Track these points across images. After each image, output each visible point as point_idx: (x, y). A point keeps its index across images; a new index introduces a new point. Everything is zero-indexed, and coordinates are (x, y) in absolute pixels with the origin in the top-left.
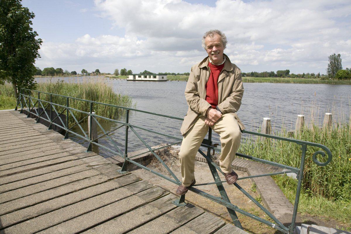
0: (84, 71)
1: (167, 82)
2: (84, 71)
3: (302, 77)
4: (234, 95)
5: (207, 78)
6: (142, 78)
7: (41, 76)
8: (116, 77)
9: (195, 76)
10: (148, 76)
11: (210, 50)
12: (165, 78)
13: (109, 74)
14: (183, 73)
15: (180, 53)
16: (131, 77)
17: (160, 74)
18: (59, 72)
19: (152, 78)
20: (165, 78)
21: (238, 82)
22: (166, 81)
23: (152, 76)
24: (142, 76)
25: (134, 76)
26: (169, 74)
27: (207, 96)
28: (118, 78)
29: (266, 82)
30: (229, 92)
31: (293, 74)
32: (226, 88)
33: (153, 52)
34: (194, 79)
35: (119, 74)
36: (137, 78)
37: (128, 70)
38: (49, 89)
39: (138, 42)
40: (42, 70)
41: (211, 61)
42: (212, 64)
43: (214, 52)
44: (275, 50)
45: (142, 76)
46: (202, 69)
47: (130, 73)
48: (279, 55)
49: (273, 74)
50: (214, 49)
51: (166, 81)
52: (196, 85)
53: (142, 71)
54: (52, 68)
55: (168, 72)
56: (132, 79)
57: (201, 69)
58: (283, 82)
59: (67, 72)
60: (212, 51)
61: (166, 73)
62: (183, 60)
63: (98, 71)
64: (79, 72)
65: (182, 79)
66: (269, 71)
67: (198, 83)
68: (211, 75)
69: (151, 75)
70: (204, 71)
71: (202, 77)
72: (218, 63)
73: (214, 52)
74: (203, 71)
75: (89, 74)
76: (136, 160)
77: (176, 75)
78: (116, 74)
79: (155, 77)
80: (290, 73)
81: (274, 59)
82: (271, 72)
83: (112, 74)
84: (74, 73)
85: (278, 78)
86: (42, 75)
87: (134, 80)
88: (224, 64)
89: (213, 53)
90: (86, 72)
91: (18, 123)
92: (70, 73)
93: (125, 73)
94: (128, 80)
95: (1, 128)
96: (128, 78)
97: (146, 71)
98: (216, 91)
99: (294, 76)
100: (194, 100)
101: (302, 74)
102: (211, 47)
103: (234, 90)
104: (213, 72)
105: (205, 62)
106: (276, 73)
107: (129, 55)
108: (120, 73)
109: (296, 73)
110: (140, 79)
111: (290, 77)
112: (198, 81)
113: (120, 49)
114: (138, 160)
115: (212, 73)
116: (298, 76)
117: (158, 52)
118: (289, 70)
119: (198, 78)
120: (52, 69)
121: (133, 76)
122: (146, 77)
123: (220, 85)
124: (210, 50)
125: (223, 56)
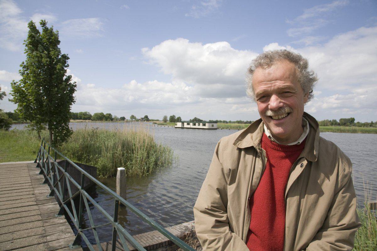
0: (133, 117)
1: (218, 130)
2: (133, 117)
3: (371, 126)
4: (332, 239)
5: (255, 180)
6: (191, 125)
7: (90, 121)
8: (165, 123)
9: (222, 170)
10: (197, 124)
11: (263, 105)
12: (215, 125)
13: (157, 120)
14: (235, 121)
15: (229, 100)
16: (179, 125)
17: (210, 122)
18: (108, 118)
19: (201, 126)
20: (215, 125)
21: (347, 197)
22: (216, 129)
23: (201, 124)
24: (191, 124)
25: (183, 123)
26: (221, 122)
27: (250, 232)
28: (166, 125)
29: (328, 131)
30: (319, 227)
31: (358, 123)
32: (308, 213)
33: (201, 99)
34: (219, 177)
35: (167, 121)
36: (186, 125)
37: (177, 117)
38: (84, 138)
39: (187, 89)
40: (92, 115)
41: (268, 133)
42: (271, 141)
43: (272, 110)
44: (334, 96)
45: (191, 124)
46: (243, 152)
47: (179, 120)
48: (337, 101)
49: (334, 123)
50: (274, 102)
51: (216, 129)
52: (222, 192)
53: (192, 118)
54: (102, 113)
55: (219, 120)
56: (181, 127)
57: (240, 150)
58: (348, 131)
59: (116, 117)
60: (266, 109)
61: (217, 120)
62: (234, 107)
63: (146, 117)
64: (128, 117)
65: (234, 127)
66: (331, 119)
67: (231, 189)
68: (267, 172)
69: (201, 123)
70: (249, 157)
71: (242, 175)
72: (287, 140)
73: (272, 110)
74: (247, 156)
75: (138, 120)
76: (159, 245)
77: (227, 123)
78: (165, 120)
79: (204, 125)
80: (356, 122)
81: (334, 106)
82: (333, 120)
83: (161, 121)
84: (123, 119)
85: (342, 127)
86: (92, 120)
87: (183, 128)
88: (304, 142)
89: (269, 113)
90: (135, 118)
91: (23, 182)
92: (118, 119)
93: (174, 120)
94: (176, 128)
95: (2, 192)
96: (176, 125)
97: (195, 118)
98: (278, 219)
99: (360, 125)
100: (213, 241)
101: (370, 122)
102: (264, 97)
103: (333, 221)
104: (272, 162)
105: (252, 132)
106: (338, 121)
107: (176, 101)
108: (168, 120)
109: (363, 121)
110: (189, 126)
111: (355, 125)
112: (230, 184)
113: (167, 95)
114: (161, 246)
115: (271, 166)
116: (366, 125)
117: (207, 99)
118: (354, 118)
119: (233, 175)
120: (102, 114)
121: (181, 123)
122: (195, 125)
123: (292, 203)
124: (263, 105)
125: (303, 120)
